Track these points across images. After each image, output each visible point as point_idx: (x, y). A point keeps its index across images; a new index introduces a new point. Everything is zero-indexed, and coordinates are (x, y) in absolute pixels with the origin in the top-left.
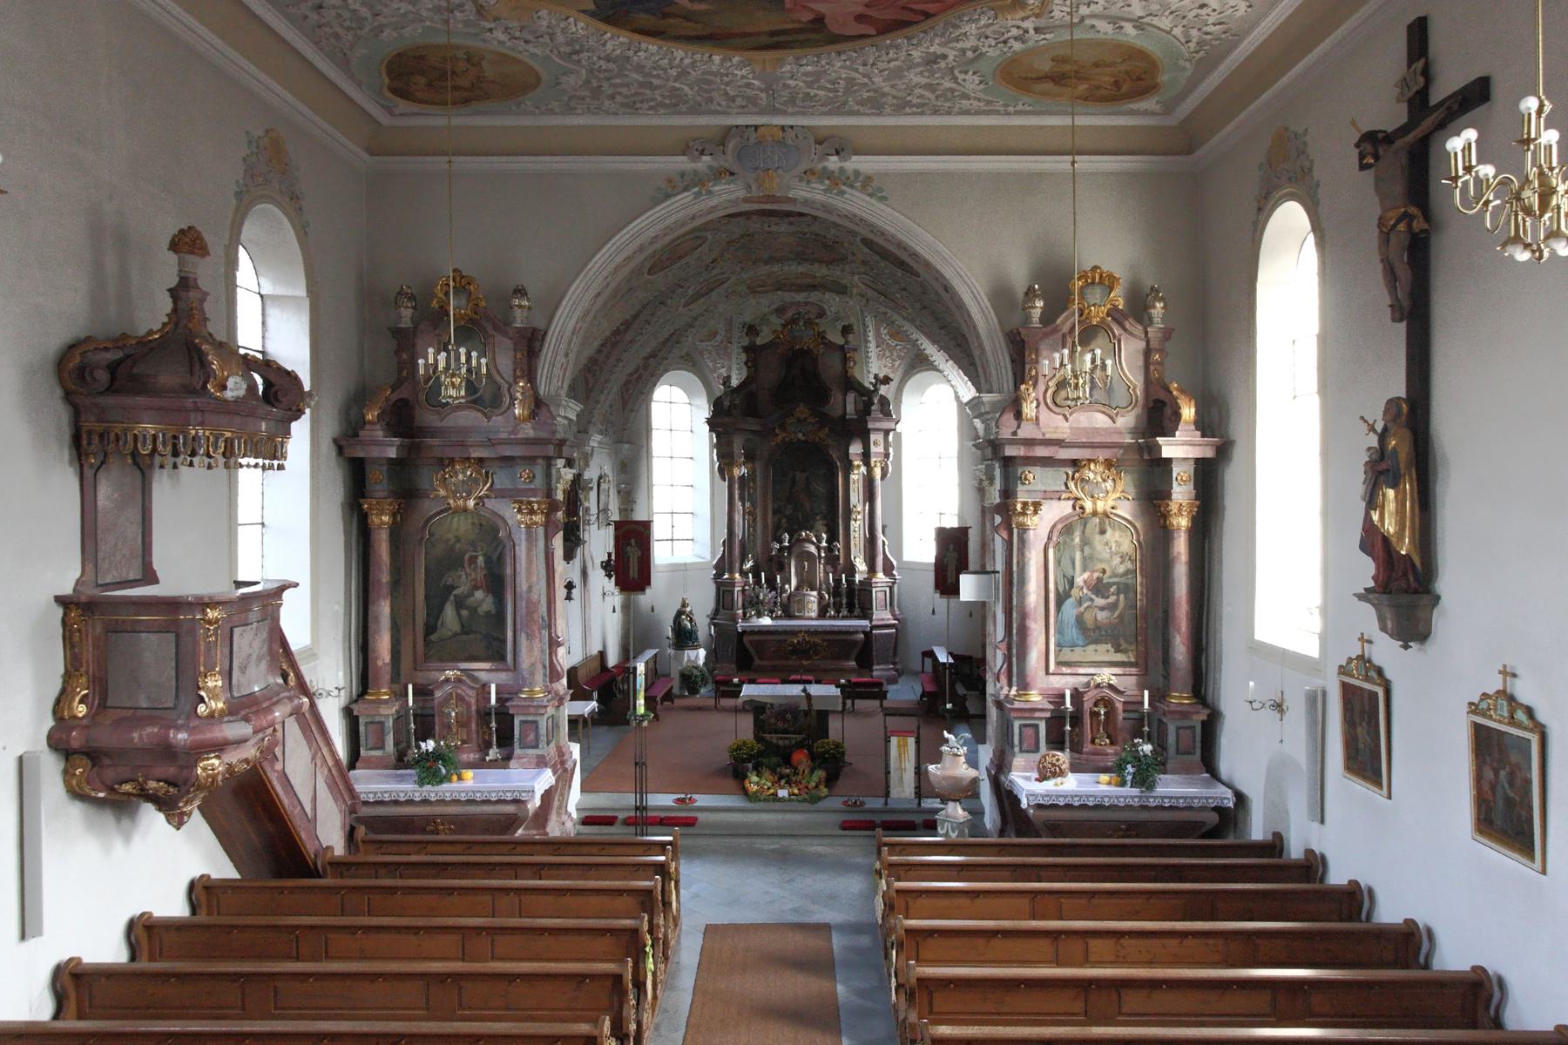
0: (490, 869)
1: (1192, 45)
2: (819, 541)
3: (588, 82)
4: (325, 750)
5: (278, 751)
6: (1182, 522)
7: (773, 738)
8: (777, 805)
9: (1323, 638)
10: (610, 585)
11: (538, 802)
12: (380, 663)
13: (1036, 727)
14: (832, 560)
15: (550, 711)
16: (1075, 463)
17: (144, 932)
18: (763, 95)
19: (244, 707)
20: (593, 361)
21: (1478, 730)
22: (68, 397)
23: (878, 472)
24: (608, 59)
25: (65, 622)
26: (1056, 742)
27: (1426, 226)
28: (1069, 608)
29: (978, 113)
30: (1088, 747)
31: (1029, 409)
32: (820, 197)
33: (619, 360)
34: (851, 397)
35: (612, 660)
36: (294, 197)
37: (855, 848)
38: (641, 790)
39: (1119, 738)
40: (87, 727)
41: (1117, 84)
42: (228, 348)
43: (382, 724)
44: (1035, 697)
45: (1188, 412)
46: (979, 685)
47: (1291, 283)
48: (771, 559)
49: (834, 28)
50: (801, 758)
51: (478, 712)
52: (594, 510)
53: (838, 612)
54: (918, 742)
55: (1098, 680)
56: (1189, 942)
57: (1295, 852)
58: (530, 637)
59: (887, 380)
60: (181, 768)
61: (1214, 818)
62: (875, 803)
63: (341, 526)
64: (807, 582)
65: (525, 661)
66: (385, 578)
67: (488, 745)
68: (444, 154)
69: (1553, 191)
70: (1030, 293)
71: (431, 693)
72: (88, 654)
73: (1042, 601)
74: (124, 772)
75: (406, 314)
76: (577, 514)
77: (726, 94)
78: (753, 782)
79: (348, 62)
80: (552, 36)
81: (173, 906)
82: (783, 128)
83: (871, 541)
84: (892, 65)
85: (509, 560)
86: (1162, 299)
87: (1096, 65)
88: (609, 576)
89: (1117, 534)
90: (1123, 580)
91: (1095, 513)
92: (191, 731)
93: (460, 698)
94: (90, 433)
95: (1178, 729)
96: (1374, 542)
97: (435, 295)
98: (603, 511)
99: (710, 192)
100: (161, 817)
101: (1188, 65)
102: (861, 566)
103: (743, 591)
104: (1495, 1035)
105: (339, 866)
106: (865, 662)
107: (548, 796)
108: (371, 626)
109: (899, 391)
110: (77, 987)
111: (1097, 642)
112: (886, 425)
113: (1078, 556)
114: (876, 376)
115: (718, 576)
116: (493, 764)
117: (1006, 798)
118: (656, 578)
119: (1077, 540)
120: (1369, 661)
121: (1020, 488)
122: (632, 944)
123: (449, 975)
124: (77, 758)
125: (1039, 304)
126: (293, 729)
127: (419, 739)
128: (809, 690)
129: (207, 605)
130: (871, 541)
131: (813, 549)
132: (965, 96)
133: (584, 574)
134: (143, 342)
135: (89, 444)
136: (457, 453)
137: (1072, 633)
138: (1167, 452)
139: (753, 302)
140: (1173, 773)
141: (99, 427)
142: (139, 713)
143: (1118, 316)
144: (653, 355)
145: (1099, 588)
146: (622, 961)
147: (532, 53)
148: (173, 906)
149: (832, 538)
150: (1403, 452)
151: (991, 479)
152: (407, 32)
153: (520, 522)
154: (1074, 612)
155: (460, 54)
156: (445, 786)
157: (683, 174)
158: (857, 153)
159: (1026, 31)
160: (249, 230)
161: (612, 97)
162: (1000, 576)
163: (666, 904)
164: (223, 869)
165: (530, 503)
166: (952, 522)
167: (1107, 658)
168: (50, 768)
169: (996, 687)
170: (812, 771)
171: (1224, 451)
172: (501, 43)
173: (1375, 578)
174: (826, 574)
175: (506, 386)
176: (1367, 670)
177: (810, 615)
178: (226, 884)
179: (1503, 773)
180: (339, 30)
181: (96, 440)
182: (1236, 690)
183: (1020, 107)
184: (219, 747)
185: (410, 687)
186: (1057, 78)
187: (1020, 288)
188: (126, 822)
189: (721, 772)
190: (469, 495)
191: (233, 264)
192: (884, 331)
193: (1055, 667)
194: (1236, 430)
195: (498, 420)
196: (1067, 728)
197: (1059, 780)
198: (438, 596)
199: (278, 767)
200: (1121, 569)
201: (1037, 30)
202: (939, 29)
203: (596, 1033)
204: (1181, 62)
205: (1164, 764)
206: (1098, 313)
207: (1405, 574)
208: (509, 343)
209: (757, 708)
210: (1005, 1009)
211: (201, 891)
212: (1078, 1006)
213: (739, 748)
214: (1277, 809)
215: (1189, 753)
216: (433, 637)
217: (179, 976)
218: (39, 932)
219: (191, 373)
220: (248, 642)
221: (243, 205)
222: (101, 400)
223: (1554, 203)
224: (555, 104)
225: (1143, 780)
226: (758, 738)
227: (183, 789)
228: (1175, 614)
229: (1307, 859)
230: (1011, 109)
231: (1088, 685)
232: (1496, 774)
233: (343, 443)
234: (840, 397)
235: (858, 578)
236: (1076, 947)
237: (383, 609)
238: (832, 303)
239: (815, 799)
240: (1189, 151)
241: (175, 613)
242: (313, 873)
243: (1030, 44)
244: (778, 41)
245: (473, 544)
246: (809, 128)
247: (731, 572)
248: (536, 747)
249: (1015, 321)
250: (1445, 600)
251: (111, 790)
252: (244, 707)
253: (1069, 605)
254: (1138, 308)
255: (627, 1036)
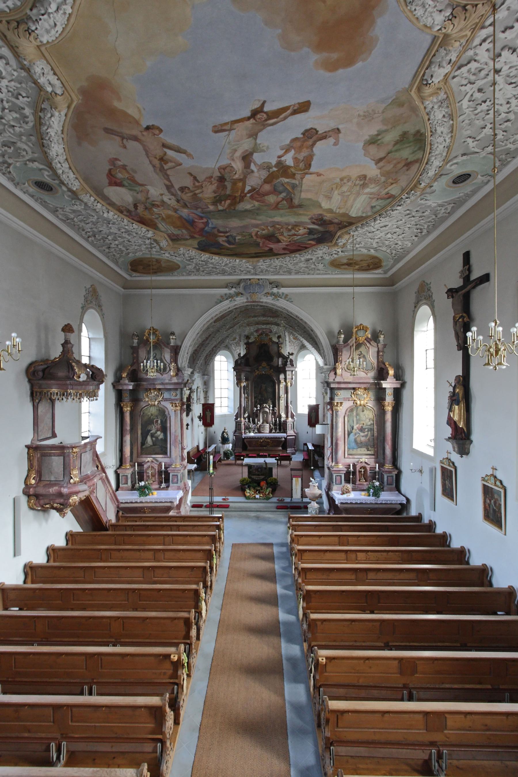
0: (162, 527)
1: (393, 255)
2: (270, 407)
3: (195, 267)
4: (109, 488)
5: (95, 491)
6: (389, 409)
7: (254, 477)
8: (255, 501)
9: (435, 448)
10: (201, 423)
11: (178, 502)
12: (126, 456)
13: (341, 476)
14: (274, 413)
15: (182, 471)
16: (354, 389)
17: (52, 552)
18: (252, 270)
19: (85, 479)
20: (196, 350)
21: (484, 486)
22: (30, 381)
23: (289, 384)
24: (202, 261)
25: (28, 453)
26: (347, 481)
27: (468, 320)
28: (352, 436)
29: (322, 274)
30: (358, 482)
31: (339, 371)
32: (272, 302)
33: (204, 350)
34: (280, 360)
35: (201, 448)
36: (100, 306)
37: (282, 516)
38: (211, 495)
39: (368, 479)
40: (35, 487)
41: (368, 266)
42: (79, 362)
43: (127, 476)
44: (341, 466)
45: (391, 372)
46: (322, 455)
47: (425, 338)
48: (254, 413)
49: (276, 252)
50: (263, 484)
51: (158, 471)
52: (195, 399)
53: (276, 431)
54: (302, 480)
55: (361, 460)
56: (390, 553)
57: (426, 521)
58: (175, 447)
59: (292, 354)
60: (65, 499)
61: (399, 507)
62: (288, 500)
63: (114, 412)
64: (266, 421)
65: (174, 455)
66: (128, 428)
67: (161, 482)
68: (150, 288)
69: (500, 350)
70: (339, 333)
71: (143, 465)
72: (35, 464)
73: (332, 683)
74: (47, 501)
75: (136, 341)
76: (190, 401)
77: (240, 270)
78: (248, 492)
79: (118, 262)
80: (184, 255)
81: (61, 542)
82: (259, 279)
83: (287, 407)
84: (295, 261)
85: (168, 422)
86: (383, 334)
87: (361, 261)
88: (200, 421)
89: (368, 412)
90: (369, 427)
91: (360, 405)
92: (69, 488)
93: (152, 467)
94: (36, 392)
95: (388, 477)
96: (451, 422)
97: (145, 335)
98: (198, 399)
99: (235, 300)
100: (58, 514)
101: (392, 260)
102: (283, 415)
103: (244, 424)
104: (489, 589)
105: (114, 527)
106: (285, 448)
107: (181, 500)
108: (124, 444)
109: (297, 356)
110: (31, 572)
111: (361, 447)
112: (292, 369)
113: (355, 419)
114: (289, 353)
115: (236, 419)
116: (163, 489)
117: (331, 500)
118: (216, 421)
119: (355, 414)
120: (450, 460)
121: (336, 397)
122: (208, 555)
123: (150, 567)
124: (32, 498)
125: (343, 336)
126: (100, 483)
127: (139, 481)
128: (265, 461)
129: (74, 447)
130: (287, 407)
131: (267, 410)
132: (318, 270)
133: (192, 420)
134: (53, 362)
135: (36, 395)
136: (152, 387)
137: (353, 444)
138: (384, 386)
139: (248, 328)
140: (387, 491)
141: (39, 390)
142: (52, 482)
143: (368, 340)
144: (215, 346)
145: (362, 430)
146: (206, 562)
147: (177, 260)
148: (61, 542)
149: (274, 406)
150: (461, 393)
151: (326, 393)
152: (137, 254)
153: (172, 410)
154: (354, 438)
155: (154, 260)
156: (148, 497)
157: (226, 294)
158: (283, 287)
159: (338, 252)
160: (86, 317)
161: (203, 271)
162: (329, 426)
163: (220, 538)
164: (77, 528)
165: (175, 403)
166: (313, 403)
167: (364, 453)
168: (24, 500)
169: (328, 462)
170: (267, 488)
171: (403, 385)
172: (168, 257)
173: (452, 434)
174: (272, 418)
175: (168, 365)
176: (449, 463)
177: (266, 433)
178: (78, 534)
179: (492, 501)
180: (115, 253)
181: (38, 394)
182: (406, 464)
183: (336, 272)
184: (76, 493)
185: (136, 464)
186: (349, 264)
187: (336, 331)
188: (46, 514)
189: (236, 489)
190: (156, 400)
191: (80, 330)
192: (291, 337)
193: (348, 455)
194: (407, 378)
195: (165, 376)
196: (350, 476)
197: (348, 494)
198: (145, 434)
199: (95, 495)
200: (369, 423)
201: (342, 251)
202: (310, 252)
203: (198, 588)
204: (389, 260)
205: (383, 488)
206: (362, 339)
207: (461, 433)
208: (169, 350)
209: (250, 467)
210: (330, 578)
211: (70, 536)
212: (353, 577)
213: (243, 481)
214: (420, 505)
215: (391, 485)
216: (144, 447)
217: (64, 568)
218: (20, 554)
219: (69, 372)
220: (87, 457)
221: (84, 309)
222: (40, 382)
223: (500, 353)
224: (184, 273)
225: (376, 494)
226: (249, 477)
227: (65, 506)
228: (387, 437)
229: (429, 523)
230: (333, 273)
231: (358, 462)
232: (490, 501)
233: (115, 384)
234: (277, 359)
235: (282, 420)
236: (353, 556)
237: (127, 438)
238: (275, 328)
239: (268, 499)
240: (393, 285)
241: (62, 449)
242: (106, 530)
243: (340, 255)
244: (257, 256)
245: (157, 416)
246: (267, 279)
247: (240, 418)
248: (177, 483)
249: (334, 342)
250: (475, 442)
251: (42, 506)
252: (85, 479)
253: (352, 435)
254: (375, 337)
255: (208, 587)
